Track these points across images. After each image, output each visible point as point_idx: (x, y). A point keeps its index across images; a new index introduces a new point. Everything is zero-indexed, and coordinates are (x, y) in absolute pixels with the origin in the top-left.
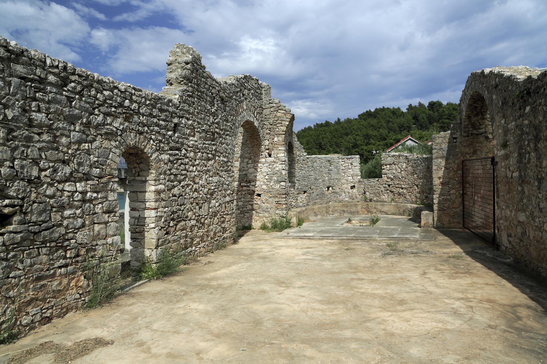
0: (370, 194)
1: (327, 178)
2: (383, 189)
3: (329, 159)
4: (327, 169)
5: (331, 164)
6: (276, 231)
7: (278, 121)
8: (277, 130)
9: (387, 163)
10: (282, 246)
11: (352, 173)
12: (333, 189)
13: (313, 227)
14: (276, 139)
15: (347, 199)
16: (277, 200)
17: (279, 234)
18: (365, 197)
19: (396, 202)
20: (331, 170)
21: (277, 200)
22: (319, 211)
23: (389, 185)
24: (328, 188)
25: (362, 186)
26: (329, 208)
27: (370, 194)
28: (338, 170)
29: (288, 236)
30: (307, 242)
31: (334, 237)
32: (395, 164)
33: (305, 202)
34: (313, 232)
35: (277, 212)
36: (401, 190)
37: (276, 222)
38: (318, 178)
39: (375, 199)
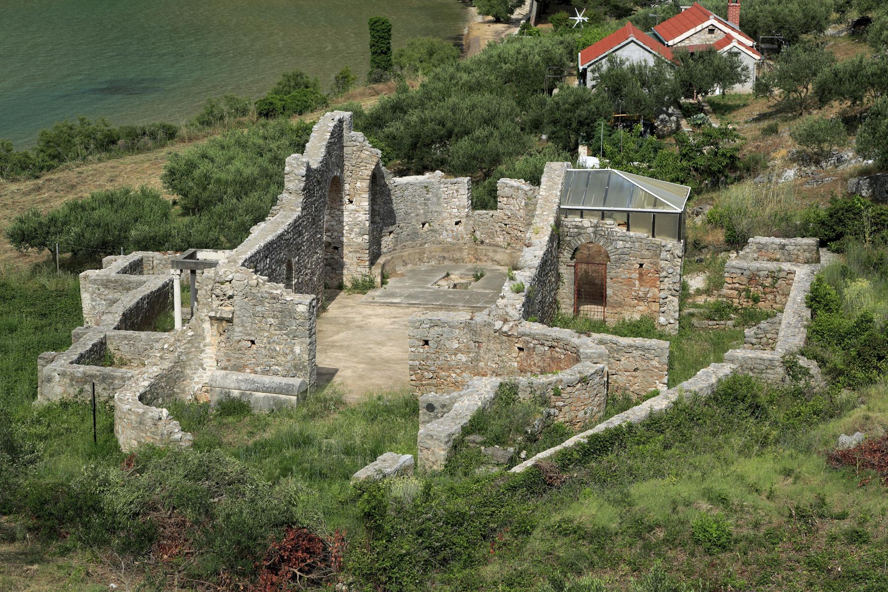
0: (482, 234)
1: (422, 211)
2: (498, 229)
3: (426, 185)
4: (423, 199)
5: (428, 191)
6: (358, 293)
7: (362, 164)
8: (361, 173)
9: (503, 194)
10: (371, 315)
11: (458, 203)
12: (430, 225)
13: (400, 287)
14: (358, 184)
15: (449, 240)
16: (358, 255)
17: (363, 298)
18: (475, 238)
19: (513, 248)
20: (428, 199)
21: (358, 255)
22: (409, 259)
23: (506, 225)
24: (424, 224)
25: (471, 222)
26: (424, 253)
27: (482, 234)
28: (438, 199)
29: (374, 303)
30: (393, 310)
31: (420, 304)
32: (513, 198)
33: (391, 246)
34: (401, 296)
35: (359, 269)
36: (519, 234)
37: (357, 281)
38: (409, 211)
39: (487, 241)
